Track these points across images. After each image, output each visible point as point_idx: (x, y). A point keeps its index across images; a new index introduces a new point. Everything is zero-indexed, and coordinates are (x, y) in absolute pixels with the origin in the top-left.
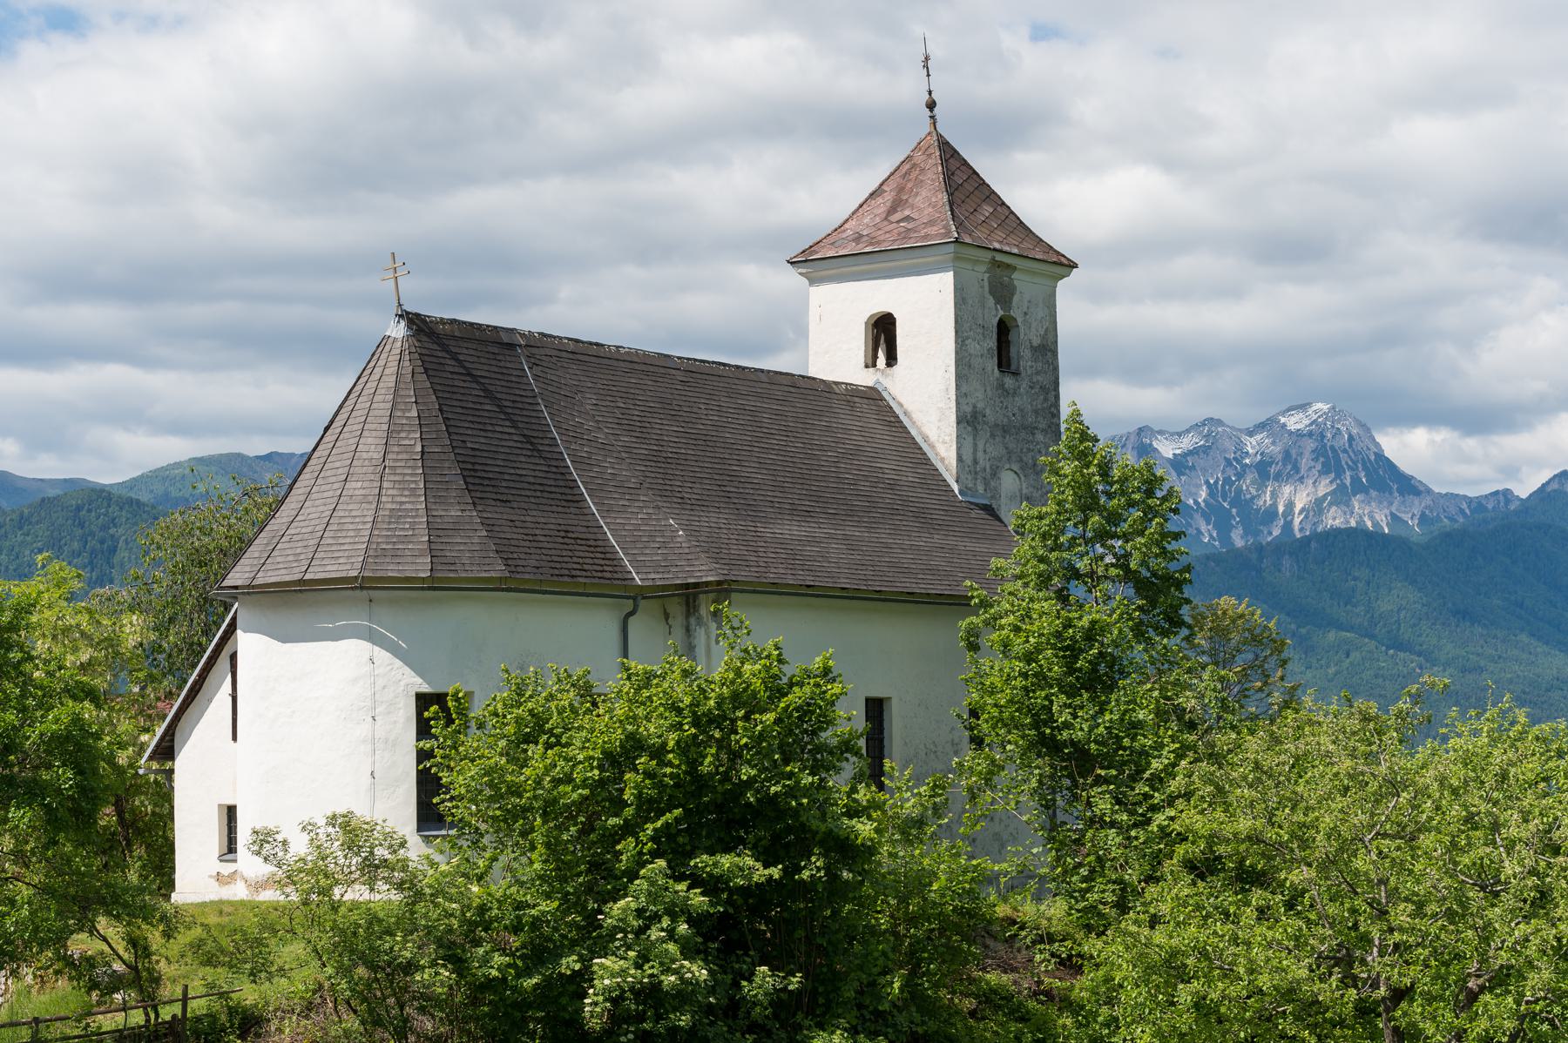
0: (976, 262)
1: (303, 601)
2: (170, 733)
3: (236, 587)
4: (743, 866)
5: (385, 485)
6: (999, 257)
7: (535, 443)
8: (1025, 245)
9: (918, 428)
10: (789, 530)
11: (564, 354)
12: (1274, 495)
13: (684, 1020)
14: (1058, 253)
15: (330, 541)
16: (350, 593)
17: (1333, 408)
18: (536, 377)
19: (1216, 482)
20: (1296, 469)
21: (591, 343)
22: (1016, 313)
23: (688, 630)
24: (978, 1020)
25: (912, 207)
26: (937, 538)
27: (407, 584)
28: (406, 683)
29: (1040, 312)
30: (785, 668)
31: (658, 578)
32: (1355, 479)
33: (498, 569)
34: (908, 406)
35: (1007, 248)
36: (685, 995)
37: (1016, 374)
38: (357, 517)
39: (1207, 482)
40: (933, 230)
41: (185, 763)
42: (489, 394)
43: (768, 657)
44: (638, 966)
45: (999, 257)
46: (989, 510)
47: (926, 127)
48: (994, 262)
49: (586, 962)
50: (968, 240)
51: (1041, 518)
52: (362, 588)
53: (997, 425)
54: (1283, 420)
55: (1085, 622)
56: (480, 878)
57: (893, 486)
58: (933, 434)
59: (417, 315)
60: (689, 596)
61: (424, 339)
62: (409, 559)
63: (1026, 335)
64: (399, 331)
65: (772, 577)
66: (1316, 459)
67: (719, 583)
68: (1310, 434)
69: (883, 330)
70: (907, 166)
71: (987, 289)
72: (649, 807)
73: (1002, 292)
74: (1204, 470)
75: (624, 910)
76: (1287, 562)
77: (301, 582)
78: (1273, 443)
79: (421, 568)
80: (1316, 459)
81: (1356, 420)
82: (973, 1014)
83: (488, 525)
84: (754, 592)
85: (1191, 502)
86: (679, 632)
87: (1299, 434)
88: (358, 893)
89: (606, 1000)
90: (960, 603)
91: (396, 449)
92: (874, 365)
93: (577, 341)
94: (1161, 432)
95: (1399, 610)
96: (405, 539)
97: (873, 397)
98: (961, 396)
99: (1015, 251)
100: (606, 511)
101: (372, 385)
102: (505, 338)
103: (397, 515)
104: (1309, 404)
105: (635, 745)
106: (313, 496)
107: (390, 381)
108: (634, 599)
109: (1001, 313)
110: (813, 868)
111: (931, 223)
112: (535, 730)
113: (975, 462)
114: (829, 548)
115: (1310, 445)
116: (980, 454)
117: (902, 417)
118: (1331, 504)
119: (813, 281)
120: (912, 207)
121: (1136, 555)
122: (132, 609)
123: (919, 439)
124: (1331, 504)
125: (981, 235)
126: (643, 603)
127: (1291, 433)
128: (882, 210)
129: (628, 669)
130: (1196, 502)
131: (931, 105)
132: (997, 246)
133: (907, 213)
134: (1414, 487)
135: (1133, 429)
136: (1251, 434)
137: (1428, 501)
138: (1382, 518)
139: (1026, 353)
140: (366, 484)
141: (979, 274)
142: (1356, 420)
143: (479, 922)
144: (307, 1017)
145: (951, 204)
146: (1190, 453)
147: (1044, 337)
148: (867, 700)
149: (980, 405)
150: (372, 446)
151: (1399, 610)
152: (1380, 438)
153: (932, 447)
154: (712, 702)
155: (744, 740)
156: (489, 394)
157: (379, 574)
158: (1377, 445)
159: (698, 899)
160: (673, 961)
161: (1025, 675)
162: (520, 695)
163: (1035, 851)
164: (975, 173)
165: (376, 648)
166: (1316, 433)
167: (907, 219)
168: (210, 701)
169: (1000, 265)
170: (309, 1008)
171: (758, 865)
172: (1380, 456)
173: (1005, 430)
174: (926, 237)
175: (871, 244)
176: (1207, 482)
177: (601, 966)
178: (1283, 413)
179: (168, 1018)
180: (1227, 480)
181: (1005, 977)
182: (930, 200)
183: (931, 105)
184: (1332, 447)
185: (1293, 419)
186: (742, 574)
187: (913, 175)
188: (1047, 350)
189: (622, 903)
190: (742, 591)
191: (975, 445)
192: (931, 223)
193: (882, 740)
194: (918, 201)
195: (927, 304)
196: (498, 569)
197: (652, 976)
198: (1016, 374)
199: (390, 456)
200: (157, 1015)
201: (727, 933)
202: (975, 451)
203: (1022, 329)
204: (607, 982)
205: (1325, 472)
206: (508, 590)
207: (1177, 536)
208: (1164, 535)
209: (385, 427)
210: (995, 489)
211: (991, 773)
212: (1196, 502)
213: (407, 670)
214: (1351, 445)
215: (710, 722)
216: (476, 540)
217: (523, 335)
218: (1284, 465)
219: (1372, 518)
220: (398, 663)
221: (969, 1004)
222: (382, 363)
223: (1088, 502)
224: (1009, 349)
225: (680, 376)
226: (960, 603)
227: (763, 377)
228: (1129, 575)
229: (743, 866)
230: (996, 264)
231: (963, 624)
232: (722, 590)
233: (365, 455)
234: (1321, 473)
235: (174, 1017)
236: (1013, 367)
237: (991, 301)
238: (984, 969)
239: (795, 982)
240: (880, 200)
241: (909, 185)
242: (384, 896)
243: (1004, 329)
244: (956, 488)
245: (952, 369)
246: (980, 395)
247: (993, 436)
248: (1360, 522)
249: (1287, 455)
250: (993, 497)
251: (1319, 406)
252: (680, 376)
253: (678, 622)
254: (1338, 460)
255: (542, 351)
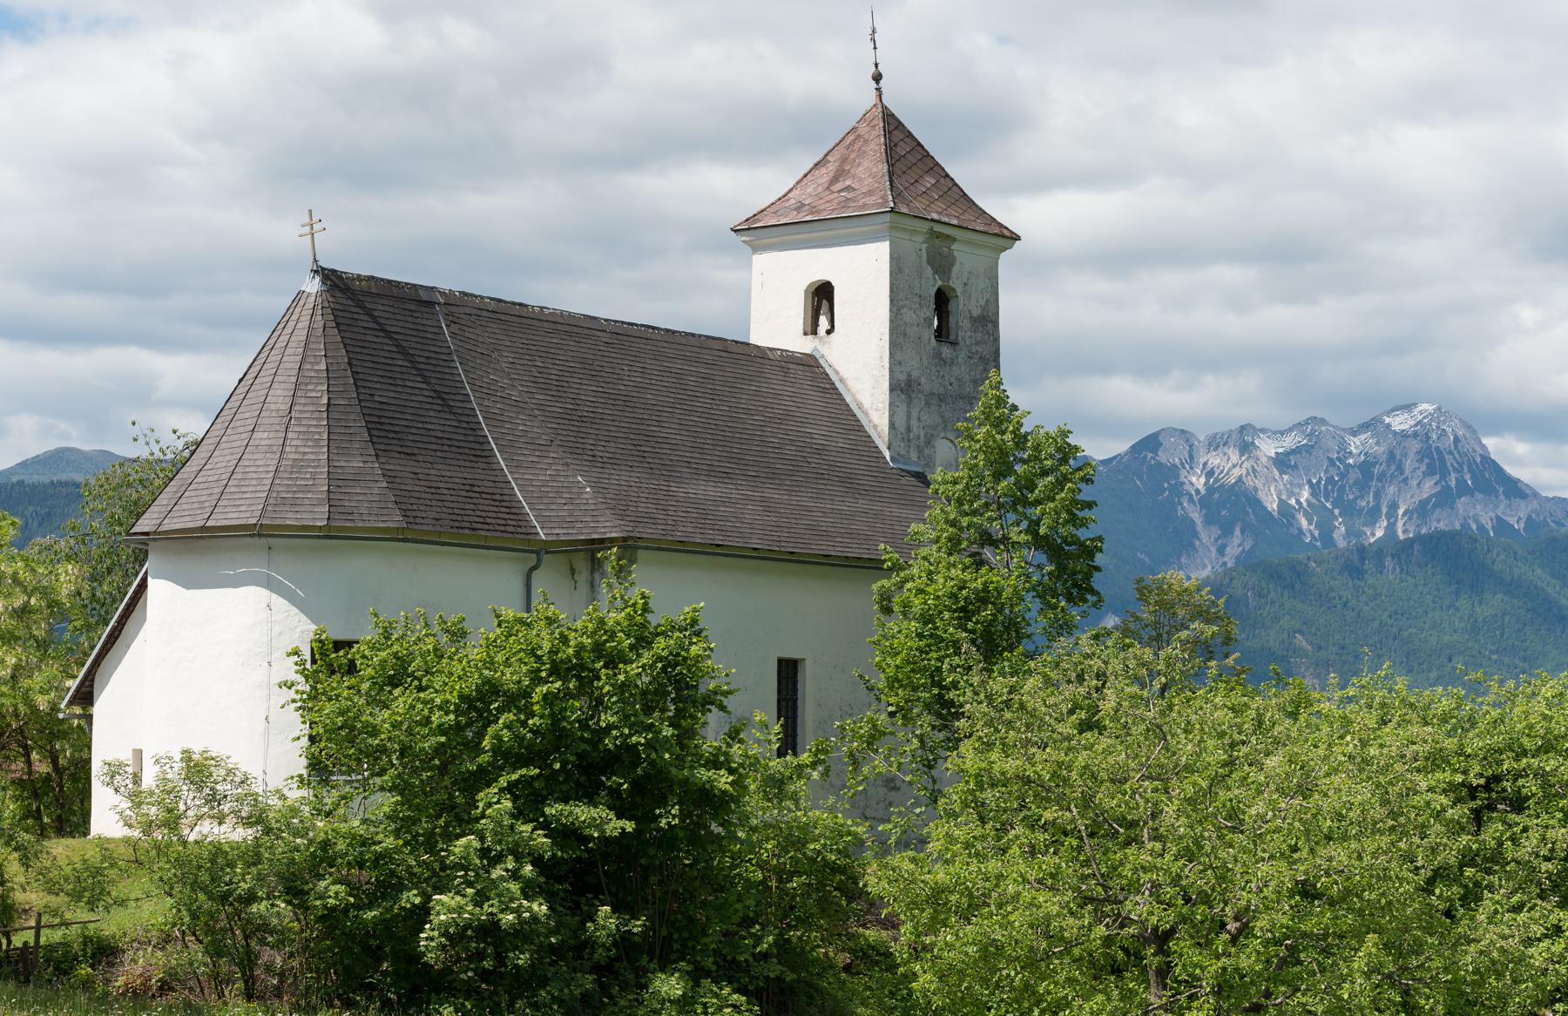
0: (914, 232)
1: (209, 547)
2: (89, 679)
3: (147, 534)
4: (596, 818)
5: (290, 435)
6: (937, 228)
7: (447, 399)
8: (966, 216)
9: (853, 395)
10: (705, 490)
11: (485, 313)
12: (1377, 496)
13: (523, 959)
14: (1001, 225)
15: (234, 489)
16: (249, 540)
17: (1439, 409)
18: (453, 335)
19: (1319, 482)
20: (1400, 469)
21: (514, 304)
22: (955, 283)
23: (592, 585)
24: (853, 975)
25: (854, 177)
26: (862, 504)
27: (303, 532)
28: (299, 630)
29: (982, 284)
30: (649, 617)
31: (563, 534)
32: (1461, 482)
33: (395, 520)
34: (844, 373)
35: (946, 219)
36: (524, 933)
37: (954, 344)
38: (261, 465)
39: (1310, 482)
40: (871, 200)
41: (102, 708)
42: (402, 351)
43: (634, 605)
44: (478, 904)
45: (937, 228)
46: (922, 479)
47: (873, 99)
48: (932, 232)
49: (427, 898)
50: (905, 210)
51: (955, 483)
52: (260, 535)
53: (932, 394)
54: (1387, 420)
55: (979, 584)
56: (328, 814)
57: (820, 451)
58: (866, 401)
59: (334, 271)
60: (592, 548)
61: (338, 294)
62: (307, 508)
63: (965, 307)
64: (313, 286)
65: (678, 535)
66: (1420, 461)
67: (625, 539)
68: (1415, 435)
69: (822, 295)
70: (851, 137)
71: (924, 258)
72: (507, 757)
73: (941, 263)
74: (1307, 470)
75: (466, 847)
76: (1389, 562)
77: (203, 528)
78: (1378, 443)
79: (318, 516)
80: (1420, 461)
81: (1461, 421)
82: (847, 968)
83: (390, 477)
84: (659, 549)
85: (1293, 502)
86: (583, 588)
87: (1403, 435)
88: (207, 830)
89: (442, 935)
90: (874, 566)
91: (303, 401)
92: (814, 332)
93: (500, 301)
94: (1263, 431)
95: (1504, 614)
96: (306, 489)
97: (810, 364)
98: (895, 364)
99: (955, 222)
100: (515, 467)
101: (284, 338)
102: (424, 296)
103: (298, 465)
104: (1415, 405)
105: (490, 690)
106: (222, 446)
107: (301, 335)
108: (537, 553)
109: (940, 283)
110: (670, 817)
111: (870, 193)
112: (397, 675)
113: (909, 430)
114: (745, 510)
115: (1415, 446)
116: (914, 422)
117: (838, 384)
118: (1435, 506)
119: (757, 249)
120: (854, 177)
121: (1046, 521)
122: (68, 558)
123: (853, 407)
124: (1435, 506)
125: (919, 206)
126: (546, 558)
127: (1395, 433)
128: (826, 179)
129: (498, 616)
130: (1298, 502)
131: (877, 78)
132: (935, 216)
133: (848, 183)
134: (1521, 490)
135: (1235, 426)
136: (1354, 433)
137: (1534, 504)
138: (1486, 519)
139: (966, 324)
140: (272, 435)
141: (917, 245)
142: (1461, 421)
143: (324, 857)
144: (163, 949)
145: (891, 174)
146: (1293, 452)
147: (984, 308)
148: (780, 661)
149: (915, 374)
150: (280, 398)
151: (1504, 614)
152: (1484, 441)
153: (866, 414)
154: (571, 651)
155: (607, 688)
156: (402, 351)
157: (277, 522)
158: (1483, 447)
159: (541, 840)
160: (512, 900)
161: (920, 636)
162: (388, 638)
163: (918, 811)
164: (919, 144)
165: (274, 596)
166: (1421, 434)
167: (848, 188)
168: (128, 647)
169: (939, 235)
170: (167, 939)
171: (612, 815)
172: (1486, 458)
173: (941, 399)
174: (864, 206)
175: (812, 213)
176: (1310, 482)
177: (439, 901)
178: (1388, 413)
179: (19, 945)
180: (1330, 480)
181: (884, 934)
182: (870, 170)
183: (877, 78)
184: (1437, 449)
185: (1398, 420)
186: (648, 531)
187: (857, 147)
188: (988, 321)
189: (463, 841)
190: (647, 548)
191: (909, 412)
192: (870, 193)
193: (795, 701)
194: (860, 171)
195: (864, 272)
196: (395, 520)
197: (491, 914)
198: (954, 344)
199: (297, 408)
200: (9, 942)
201: (575, 875)
202: (909, 418)
203: (961, 299)
204: (443, 917)
205: (1430, 472)
206: (405, 540)
207: (1090, 505)
208: (1074, 502)
209: (294, 379)
210: (930, 457)
211: (872, 737)
212: (1298, 502)
213: (303, 617)
214: (1456, 447)
215: (577, 671)
216: (376, 491)
217: (443, 294)
218: (1388, 466)
219: (1476, 521)
220: (295, 610)
221: (843, 958)
222: (295, 317)
223: (1001, 466)
224: (947, 319)
225: (605, 337)
226: (874, 566)
227: (694, 341)
228: (1039, 542)
229: (596, 818)
230: (934, 235)
231: (875, 587)
232: (629, 547)
233: (273, 407)
234: (1426, 474)
235: (25, 943)
236: (952, 337)
237: (929, 271)
238: (864, 926)
239: (637, 926)
240: (823, 170)
241: (853, 156)
242: (235, 834)
243: (942, 301)
244: (887, 455)
245: (887, 337)
246: (915, 363)
247: (928, 404)
248: (1465, 525)
249: (1391, 455)
250: (926, 465)
251: (1425, 406)
252: (605, 337)
253: (583, 577)
254: (1442, 460)
255: (461, 310)
